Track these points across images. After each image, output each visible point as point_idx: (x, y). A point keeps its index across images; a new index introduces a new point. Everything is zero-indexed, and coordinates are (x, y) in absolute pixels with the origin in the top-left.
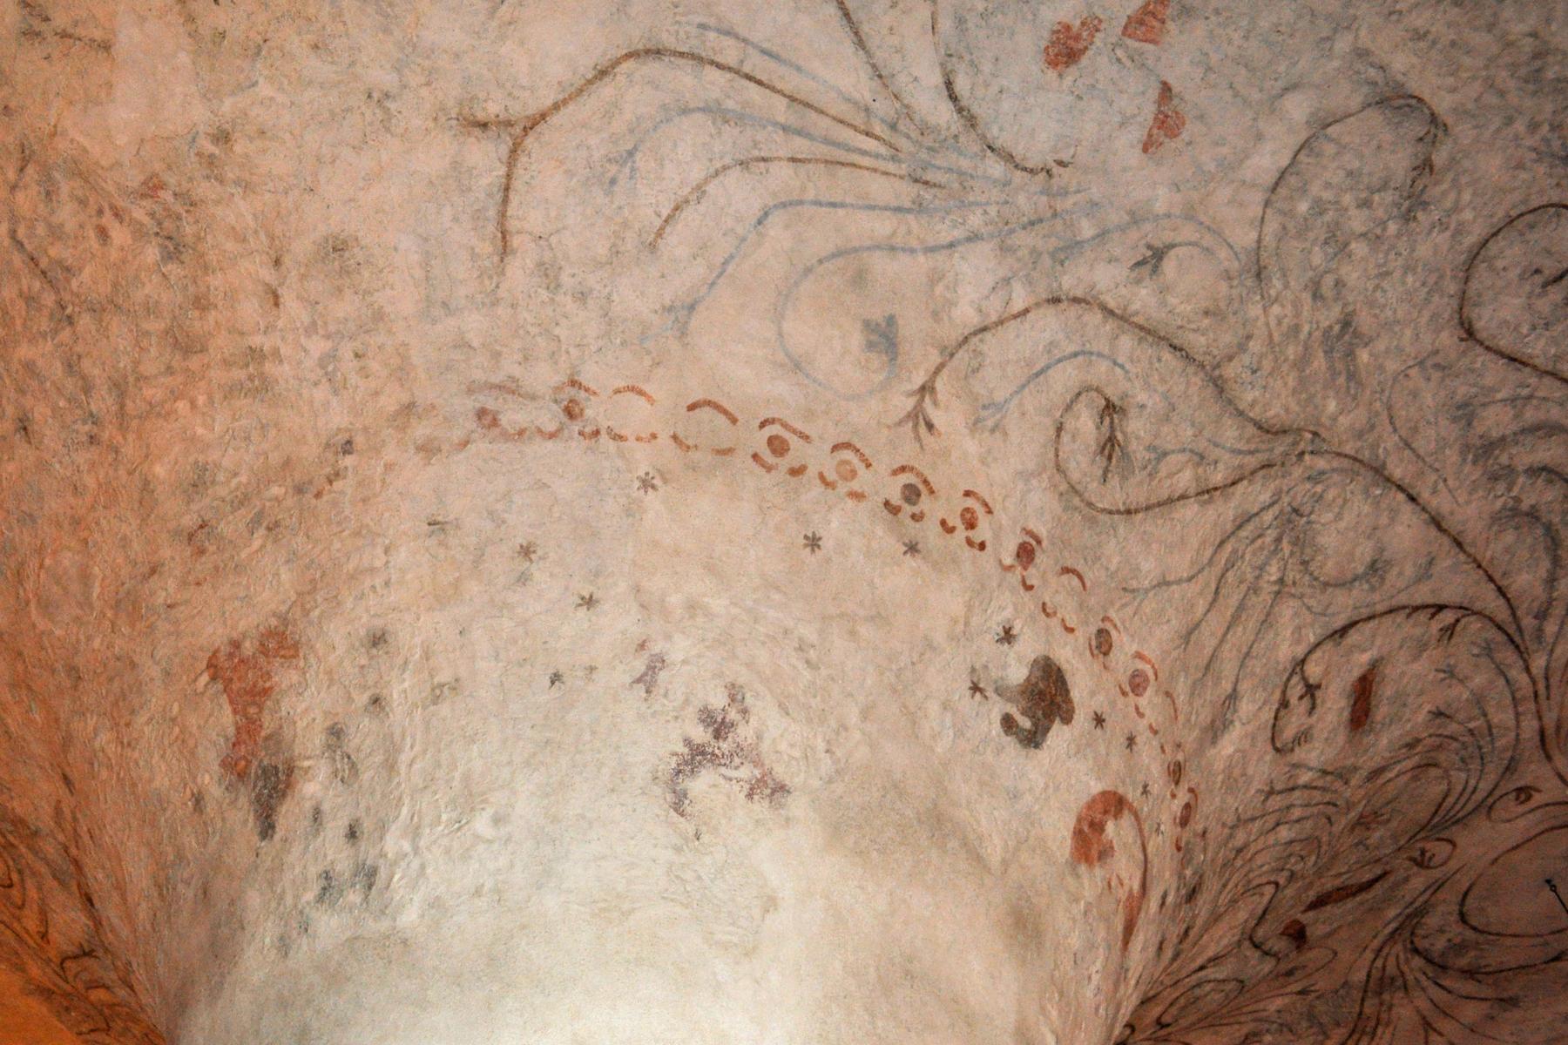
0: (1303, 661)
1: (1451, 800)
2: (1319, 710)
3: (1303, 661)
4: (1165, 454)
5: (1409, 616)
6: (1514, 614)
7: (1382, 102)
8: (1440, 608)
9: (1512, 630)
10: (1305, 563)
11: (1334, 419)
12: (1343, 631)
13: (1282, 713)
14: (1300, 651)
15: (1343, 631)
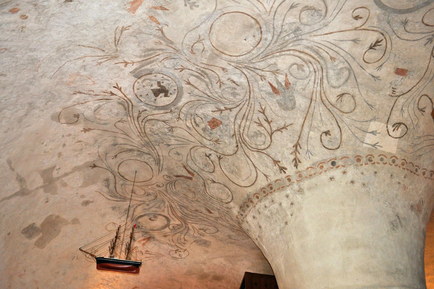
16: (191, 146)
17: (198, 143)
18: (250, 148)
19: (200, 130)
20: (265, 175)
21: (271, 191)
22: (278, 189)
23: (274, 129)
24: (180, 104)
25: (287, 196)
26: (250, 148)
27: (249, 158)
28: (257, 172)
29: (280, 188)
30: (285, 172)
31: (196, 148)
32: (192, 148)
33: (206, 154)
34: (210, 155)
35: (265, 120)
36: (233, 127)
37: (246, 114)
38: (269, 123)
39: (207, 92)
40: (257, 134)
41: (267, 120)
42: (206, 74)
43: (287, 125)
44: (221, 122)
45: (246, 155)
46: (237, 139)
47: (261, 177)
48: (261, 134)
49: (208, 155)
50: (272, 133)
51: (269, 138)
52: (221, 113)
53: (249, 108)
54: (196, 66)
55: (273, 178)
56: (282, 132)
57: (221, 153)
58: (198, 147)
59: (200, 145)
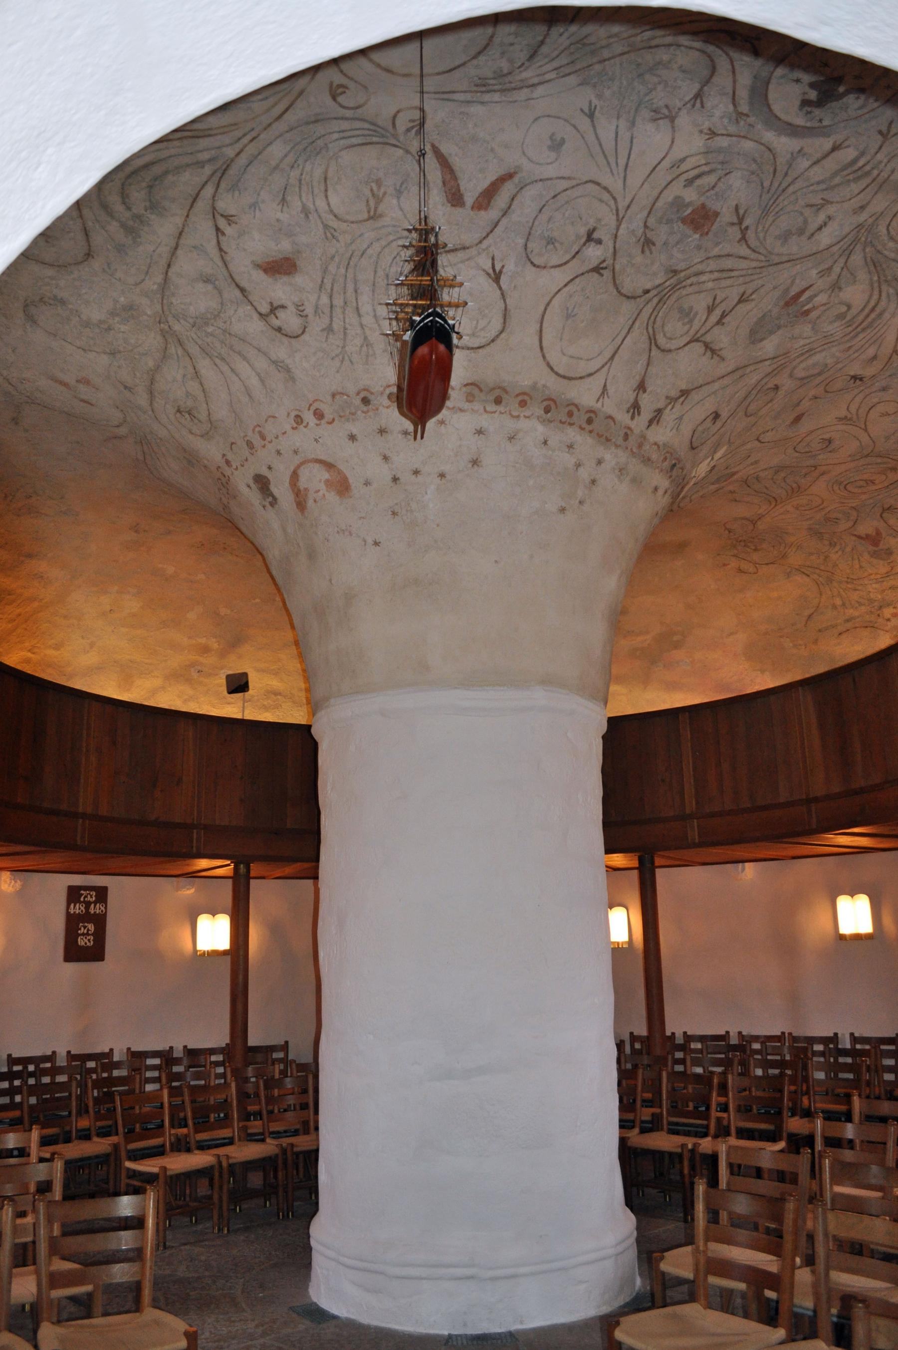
0: (260, 314)
1: (354, 141)
2: (283, 302)
3: (260, 314)
4: (187, 392)
5: (226, 253)
6: (206, 182)
7: (34, 322)
8: (218, 229)
9: (215, 179)
10: (215, 318)
11: (149, 316)
12: (242, 290)
13: (283, 332)
14: (256, 316)
15: (242, 290)
16: (607, 180)
17: (628, 200)
18: (653, 318)
19: (677, 189)
20: (605, 386)
21: (584, 425)
22: (598, 434)
23: (708, 338)
24: (769, 136)
25: (599, 462)
26: (653, 318)
27: (628, 332)
28: (603, 366)
29: (602, 436)
30: (632, 418)
31: (606, 196)
32: (598, 184)
33: (594, 230)
34: (599, 242)
35: (724, 311)
36: (696, 261)
37: (733, 274)
38: (720, 322)
39: (799, 184)
40: (688, 314)
41: (723, 315)
42: (859, 178)
43: (720, 353)
44: (707, 233)
45: (634, 323)
46: (668, 283)
47: (596, 384)
48: (691, 321)
49: (595, 235)
50: (697, 340)
51: (688, 339)
52: (733, 224)
53: (750, 272)
54: (885, 161)
55: (609, 407)
56: (704, 354)
57: (617, 267)
58: (612, 202)
59: (622, 205)
